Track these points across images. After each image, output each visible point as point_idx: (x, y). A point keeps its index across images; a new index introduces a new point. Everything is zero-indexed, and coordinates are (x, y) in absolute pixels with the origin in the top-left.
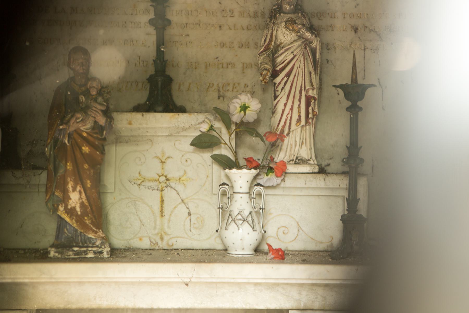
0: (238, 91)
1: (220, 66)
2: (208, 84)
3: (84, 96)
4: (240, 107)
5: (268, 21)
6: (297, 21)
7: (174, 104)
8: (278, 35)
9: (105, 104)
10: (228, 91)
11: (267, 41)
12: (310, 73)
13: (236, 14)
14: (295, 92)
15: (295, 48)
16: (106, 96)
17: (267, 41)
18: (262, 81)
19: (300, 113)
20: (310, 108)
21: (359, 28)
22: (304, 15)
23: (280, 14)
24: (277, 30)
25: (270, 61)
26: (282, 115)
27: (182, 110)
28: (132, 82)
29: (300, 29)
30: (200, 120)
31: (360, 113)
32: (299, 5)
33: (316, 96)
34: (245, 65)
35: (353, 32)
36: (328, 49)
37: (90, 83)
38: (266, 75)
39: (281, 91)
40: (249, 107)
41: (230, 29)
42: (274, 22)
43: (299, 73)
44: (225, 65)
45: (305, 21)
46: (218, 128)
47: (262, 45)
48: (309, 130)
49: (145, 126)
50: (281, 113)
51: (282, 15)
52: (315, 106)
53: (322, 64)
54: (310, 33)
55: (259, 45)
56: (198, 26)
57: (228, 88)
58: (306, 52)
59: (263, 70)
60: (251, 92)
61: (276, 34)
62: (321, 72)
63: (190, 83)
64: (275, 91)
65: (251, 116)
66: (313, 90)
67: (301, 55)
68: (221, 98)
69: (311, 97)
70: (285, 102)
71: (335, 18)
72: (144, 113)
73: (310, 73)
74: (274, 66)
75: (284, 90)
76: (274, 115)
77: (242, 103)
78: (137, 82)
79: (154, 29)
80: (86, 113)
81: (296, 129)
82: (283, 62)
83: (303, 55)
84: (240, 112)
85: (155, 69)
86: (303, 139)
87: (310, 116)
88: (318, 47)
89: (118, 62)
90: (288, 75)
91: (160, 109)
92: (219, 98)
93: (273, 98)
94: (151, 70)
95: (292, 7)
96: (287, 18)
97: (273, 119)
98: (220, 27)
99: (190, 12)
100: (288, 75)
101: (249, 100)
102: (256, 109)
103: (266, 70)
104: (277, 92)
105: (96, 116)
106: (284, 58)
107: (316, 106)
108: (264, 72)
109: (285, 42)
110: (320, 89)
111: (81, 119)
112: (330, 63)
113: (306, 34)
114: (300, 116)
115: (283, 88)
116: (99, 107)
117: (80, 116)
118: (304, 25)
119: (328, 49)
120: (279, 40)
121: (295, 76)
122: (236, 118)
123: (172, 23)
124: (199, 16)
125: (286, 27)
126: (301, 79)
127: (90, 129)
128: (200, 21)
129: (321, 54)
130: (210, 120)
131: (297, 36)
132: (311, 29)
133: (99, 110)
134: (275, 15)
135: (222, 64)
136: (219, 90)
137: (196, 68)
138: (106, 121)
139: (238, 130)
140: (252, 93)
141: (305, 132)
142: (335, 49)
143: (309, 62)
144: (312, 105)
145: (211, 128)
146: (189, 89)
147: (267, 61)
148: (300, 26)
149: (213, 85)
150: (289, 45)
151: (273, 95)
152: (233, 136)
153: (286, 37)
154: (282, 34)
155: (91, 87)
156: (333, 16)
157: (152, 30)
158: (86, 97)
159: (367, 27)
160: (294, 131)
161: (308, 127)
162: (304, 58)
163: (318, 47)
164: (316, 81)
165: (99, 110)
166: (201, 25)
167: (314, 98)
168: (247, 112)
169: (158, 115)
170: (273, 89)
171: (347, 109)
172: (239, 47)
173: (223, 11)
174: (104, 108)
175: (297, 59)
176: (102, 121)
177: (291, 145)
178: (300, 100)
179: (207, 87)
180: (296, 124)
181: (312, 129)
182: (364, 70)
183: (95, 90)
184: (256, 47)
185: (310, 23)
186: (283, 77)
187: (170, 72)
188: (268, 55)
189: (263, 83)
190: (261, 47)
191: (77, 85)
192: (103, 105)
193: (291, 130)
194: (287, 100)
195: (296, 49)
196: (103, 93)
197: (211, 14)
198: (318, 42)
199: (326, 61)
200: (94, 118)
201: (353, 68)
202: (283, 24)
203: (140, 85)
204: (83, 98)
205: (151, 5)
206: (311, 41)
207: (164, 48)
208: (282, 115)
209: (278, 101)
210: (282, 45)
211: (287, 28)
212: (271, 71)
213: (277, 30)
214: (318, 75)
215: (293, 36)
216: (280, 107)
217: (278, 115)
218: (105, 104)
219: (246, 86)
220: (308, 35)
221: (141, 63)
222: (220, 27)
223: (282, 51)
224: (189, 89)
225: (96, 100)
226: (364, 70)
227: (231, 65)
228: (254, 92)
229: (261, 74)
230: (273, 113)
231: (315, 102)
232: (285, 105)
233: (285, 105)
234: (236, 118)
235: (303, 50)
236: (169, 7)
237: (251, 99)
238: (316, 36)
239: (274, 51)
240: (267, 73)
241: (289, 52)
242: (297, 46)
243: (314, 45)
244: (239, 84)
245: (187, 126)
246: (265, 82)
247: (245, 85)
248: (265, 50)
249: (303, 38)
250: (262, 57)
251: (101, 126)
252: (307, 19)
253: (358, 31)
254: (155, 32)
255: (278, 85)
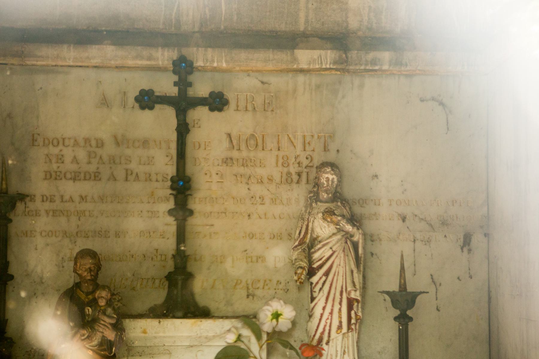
0: (269, 289)
1: (250, 260)
2: (235, 281)
3: (90, 307)
4: (272, 315)
5: (303, 211)
6: (336, 212)
8: (314, 227)
10: (258, 288)
11: (302, 234)
12: (352, 272)
13: (267, 201)
14: (335, 294)
15: (334, 242)
17: (302, 234)
18: (296, 281)
19: (341, 318)
20: (353, 313)
21: (407, 217)
22: (344, 204)
23: (316, 202)
24: (313, 221)
25: (305, 258)
26: (320, 320)
27: (204, 313)
29: (339, 221)
30: (227, 328)
31: (410, 323)
32: (338, 192)
33: (359, 298)
35: (401, 221)
36: (372, 241)
37: (98, 292)
38: (302, 274)
39: (319, 292)
41: (260, 218)
42: (309, 213)
43: (341, 269)
44: (254, 259)
45: (345, 210)
46: (246, 337)
47: (296, 237)
48: (352, 336)
49: (161, 334)
50: (319, 317)
51: (319, 203)
52: (358, 310)
53: (365, 260)
54: (351, 225)
55: (293, 236)
56: (224, 214)
57: (258, 285)
58: (346, 247)
59: (298, 268)
60: (284, 290)
61: (313, 225)
62: (364, 269)
64: (312, 291)
65: (284, 324)
66: (355, 291)
67: (341, 251)
68: (251, 297)
69: (354, 299)
70: (323, 305)
71: (379, 205)
72: (161, 320)
73: (352, 272)
74: (310, 262)
75: (321, 292)
76: (311, 320)
78: (154, 279)
79: (175, 220)
80: (92, 328)
81: (336, 338)
82: (321, 259)
83: (344, 251)
84: (272, 320)
85: (175, 266)
86: (345, 347)
87: (353, 321)
88: (361, 241)
90: (327, 274)
91: (180, 314)
92: (248, 296)
93: (310, 300)
94: (170, 266)
95: (330, 195)
96: (325, 207)
97: (310, 323)
98: (249, 216)
99: (214, 199)
100: (327, 274)
102: (290, 317)
103: (301, 267)
104: (314, 293)
106: (321, 254)
107: (360, 309)
108: (299, 271)
109: (323, 236)
110: (364, 288)
111: (86, 336)
112: (374, 256)
113: (347, 226)
114: (341, 322)
115: (321, 289)
116: (108, 320)
118: (343, 216)
119: (372, 241)
120: (316, 234)
121: (334, 275)
122: (267, 325)
123: (195, 211)
124: (226, 204)
125: (324, 219)
126: (341, 278)
127: (96, 346)
128: (226, 209)
129: (364, 248)
130: (236, 328)
131: (336, 228)
132: (354, 220)
133: (108, 323)
134: (311, 205)
135: (252, 257)
136: (248, 289)
137: (221, 262)
138: (116, 335)
139: (269, 342)
140: (286, 290)
141: (348, 340)
142: (380, 240)
143: (351, 258)
144: (355, 309)
145: (239, 338)
147: (302, 257)
148: (339, 218)
149: (241, 282)
150: (327, 239)
151: (310, 295)
152: (265, 347)
153: (323, 230)
154: (319, 227)
155: (99, 298)
156: (377, 203)
157: (171, 220)
158: (93, 308)
159: (416, 216)
160: (335, 340)
161: (350, 334)
162: (344, 255)
163: (361, 241)
164: (359, 280)
165: (108, 323)
166: (227, 214)
167: (357, 301)
169: (178, 322)
170: (310, 289)
171: (396, 319)
172: (270, 238)
173: (252, 197)
174: (113, 321)
175: (337, 256)
176: (111, 335)
177: (331, 355)
178: (340, 304)
180: (337, 331)
181: (356, 336)
182: (415, 265)
183: (104, 300)
184: (290, 238)
185: (351, 212)
186: (321, 276)
187: (191, 267)
188: (304, 250)
189: (298, 283)
190: (295, 240)
191: (83, 292)
192: (113, 317)
193: (331, 338)
194: (326, 303)
195: (336, 244)
197: (239, 201)
198: (361, 236)
199: (370, 255)
200: (102, 333)
201: (401, 271)
202: (320, 215)
203: (157, 282)
204: (90, 310)
205: (170, 194)
206: (352, 233)
207: (185, 247)
208: (320, 320)
209: (316, 304)
210: (320, 239)
211: (324, 219)
212: (307, 269)
213: (313, 221)
214: (362, 273)
215: (332, 229)
216: (318, 311)
217: (315, 319)
218: (115, 316)
219: (279, 282)
220: (349, 228)
221: (159, 257)
222: (249, 216)
223: (319, 246)
225: (104, 313)
226: (415, 265)
227: (261, 259)
228: (288, 290)
229: (296, 273)
230: (310, 316)
231: (358, 306)
232: (324, 308)
233: (324, 308)
234: (267, 325)
235: (343, 244)
236: (191, 195)
237: (284, 307)
238: (358, 229)
239: (310, 245)
240: (302, 272)
241: (327, 247)
242: (336, 240)
243: (355, 239)
244: (270, 280)
245: (211, 334)
246: (300, 283)
247: (278, 281)
248: (300, 244)
249: (343, 231)
250: (296, 253)
251: (110, 341)
252: (347, 208)
253: (407, 220)
254: (175, 223)
255: (315, 286)
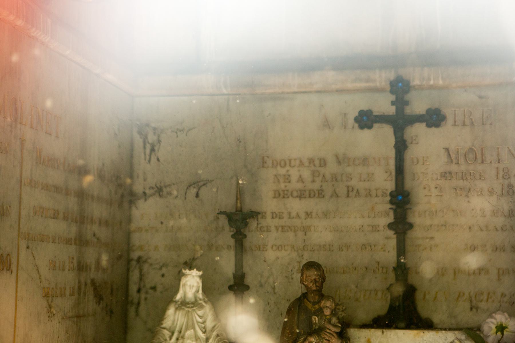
7: (419, 317)
9: (340, 325)
16: (341, 315)
27: (427, 325)
28: (371, 291)
34: (501, 272)
37: (323, 302)
40: (506, 327)
57: (482, 298)
63: (437, 293)
68: (474, 310)
72: (384, 330)
77: (498, 323)
78: (376, 291)
84: (496, 333)
89: (355, 269)
91: (402, 325)
92: (471, 309)
101: (506, 319)
105: (330, 339)
116: (334, 329)
117: (313, 339)
136: (471, 301)
146: (435, 299)
149: (464, 294)
155: (324, 307)
157: (391, 233)
158: (319, 317)
168: (505, 333)
172: (493, 250)
174: (338, 330)
179: (457, 296)
183: (329, 310)
196: (338, 311)
197: (459, 214)
204: (317, 319)
205: (390, 209)
218: (340, 325)
221: (381, 269)
224: (435, 299)
236: (410, 209)
237: (509, 319)
254: (395, 236)
